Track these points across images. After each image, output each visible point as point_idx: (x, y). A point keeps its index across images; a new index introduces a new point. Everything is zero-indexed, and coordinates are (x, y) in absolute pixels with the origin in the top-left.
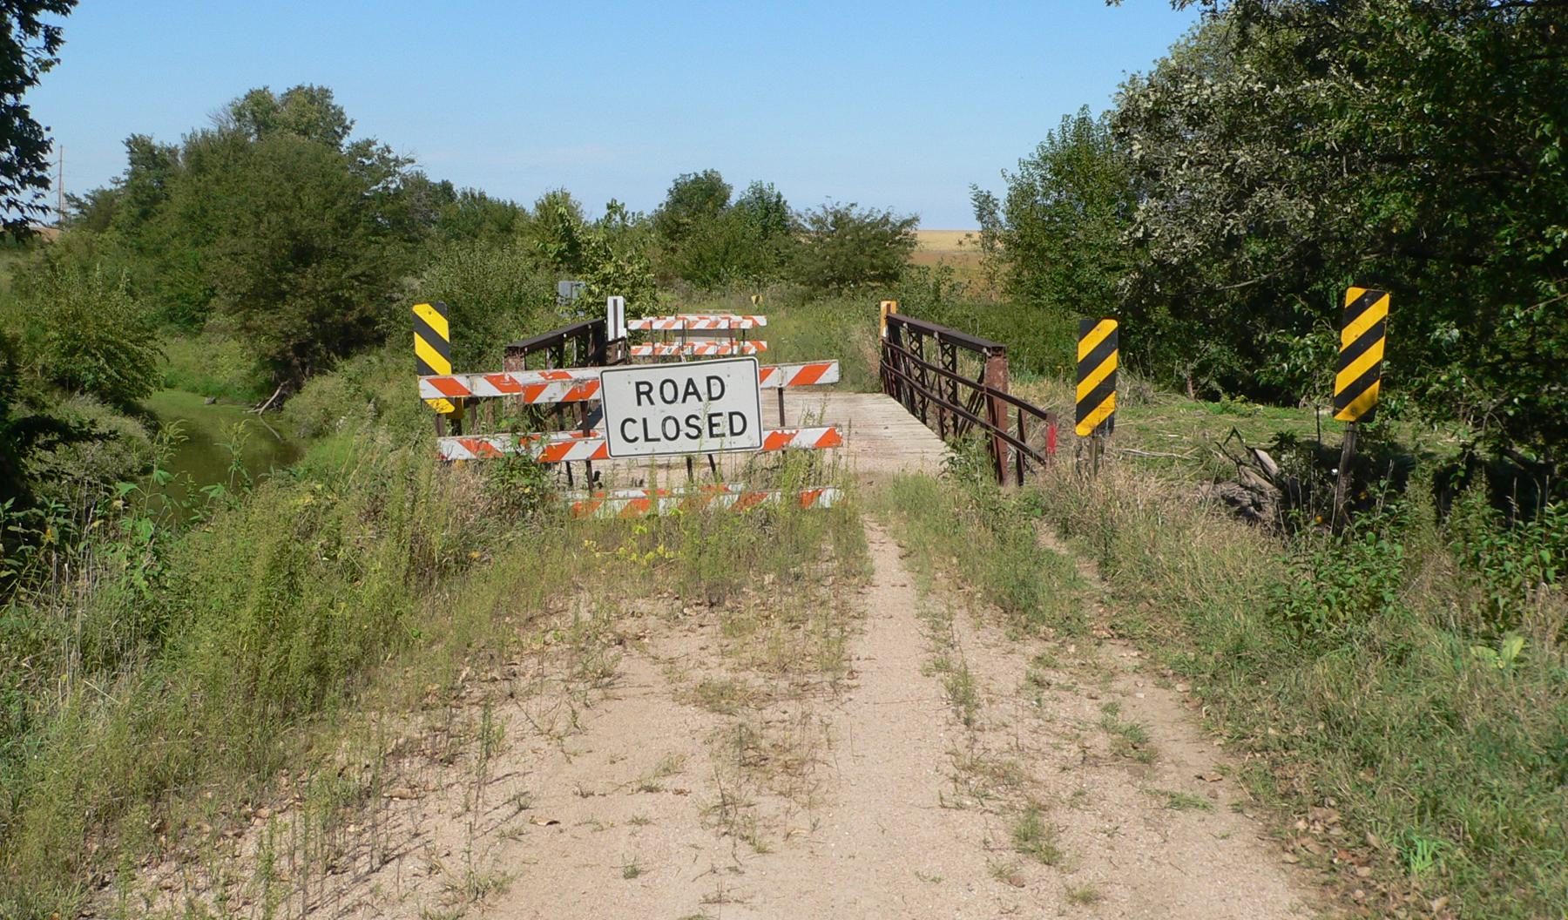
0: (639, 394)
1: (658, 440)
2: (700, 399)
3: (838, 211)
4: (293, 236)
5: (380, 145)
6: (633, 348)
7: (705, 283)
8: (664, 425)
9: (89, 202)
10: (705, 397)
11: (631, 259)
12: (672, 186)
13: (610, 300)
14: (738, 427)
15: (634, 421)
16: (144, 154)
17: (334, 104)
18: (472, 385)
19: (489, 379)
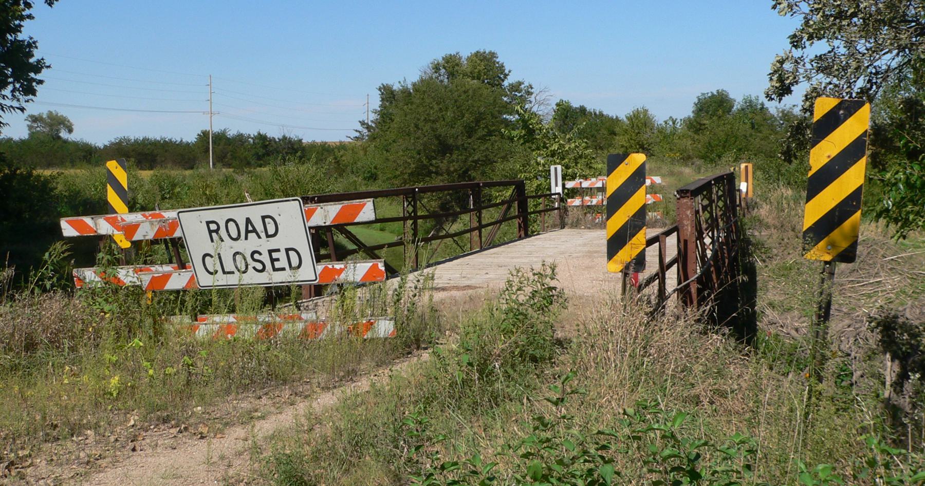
0: (210, 232)
1: (233, 273)
2: (259, 237)
3: (785, 110)
4: (438, 137)
5: (526, 84)
6: (569, 200)
7: (712, 161)
8: (234, 260)
9: (373, 125)
10: (263, 235)
11: (570, 140)
12: (696, 101)
13: (552, 168)
14: (295, 262)
15: (212, 257)
16: (388, 94)
17: (497, 60)
18: (96, 224)
19: (107, 220)
